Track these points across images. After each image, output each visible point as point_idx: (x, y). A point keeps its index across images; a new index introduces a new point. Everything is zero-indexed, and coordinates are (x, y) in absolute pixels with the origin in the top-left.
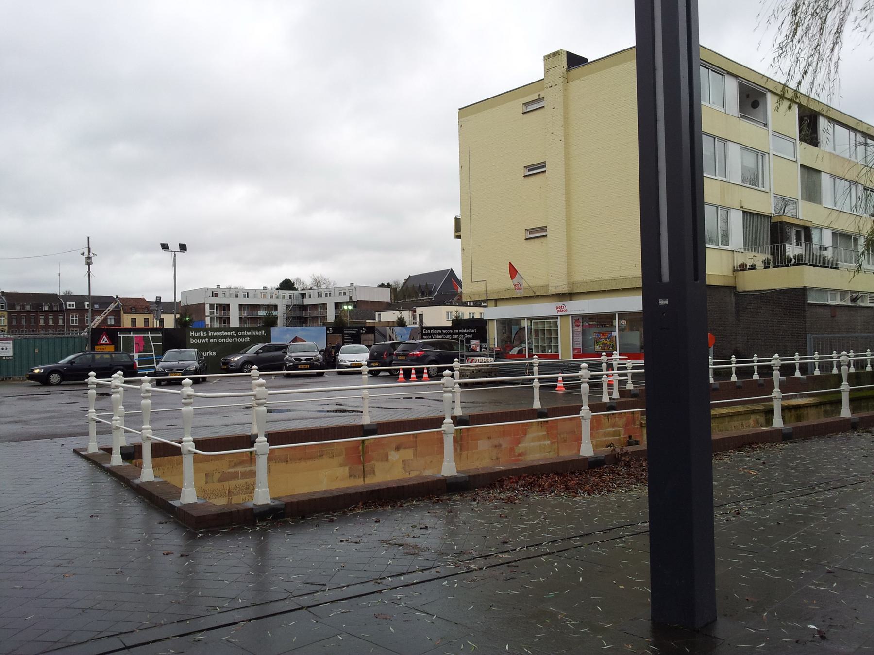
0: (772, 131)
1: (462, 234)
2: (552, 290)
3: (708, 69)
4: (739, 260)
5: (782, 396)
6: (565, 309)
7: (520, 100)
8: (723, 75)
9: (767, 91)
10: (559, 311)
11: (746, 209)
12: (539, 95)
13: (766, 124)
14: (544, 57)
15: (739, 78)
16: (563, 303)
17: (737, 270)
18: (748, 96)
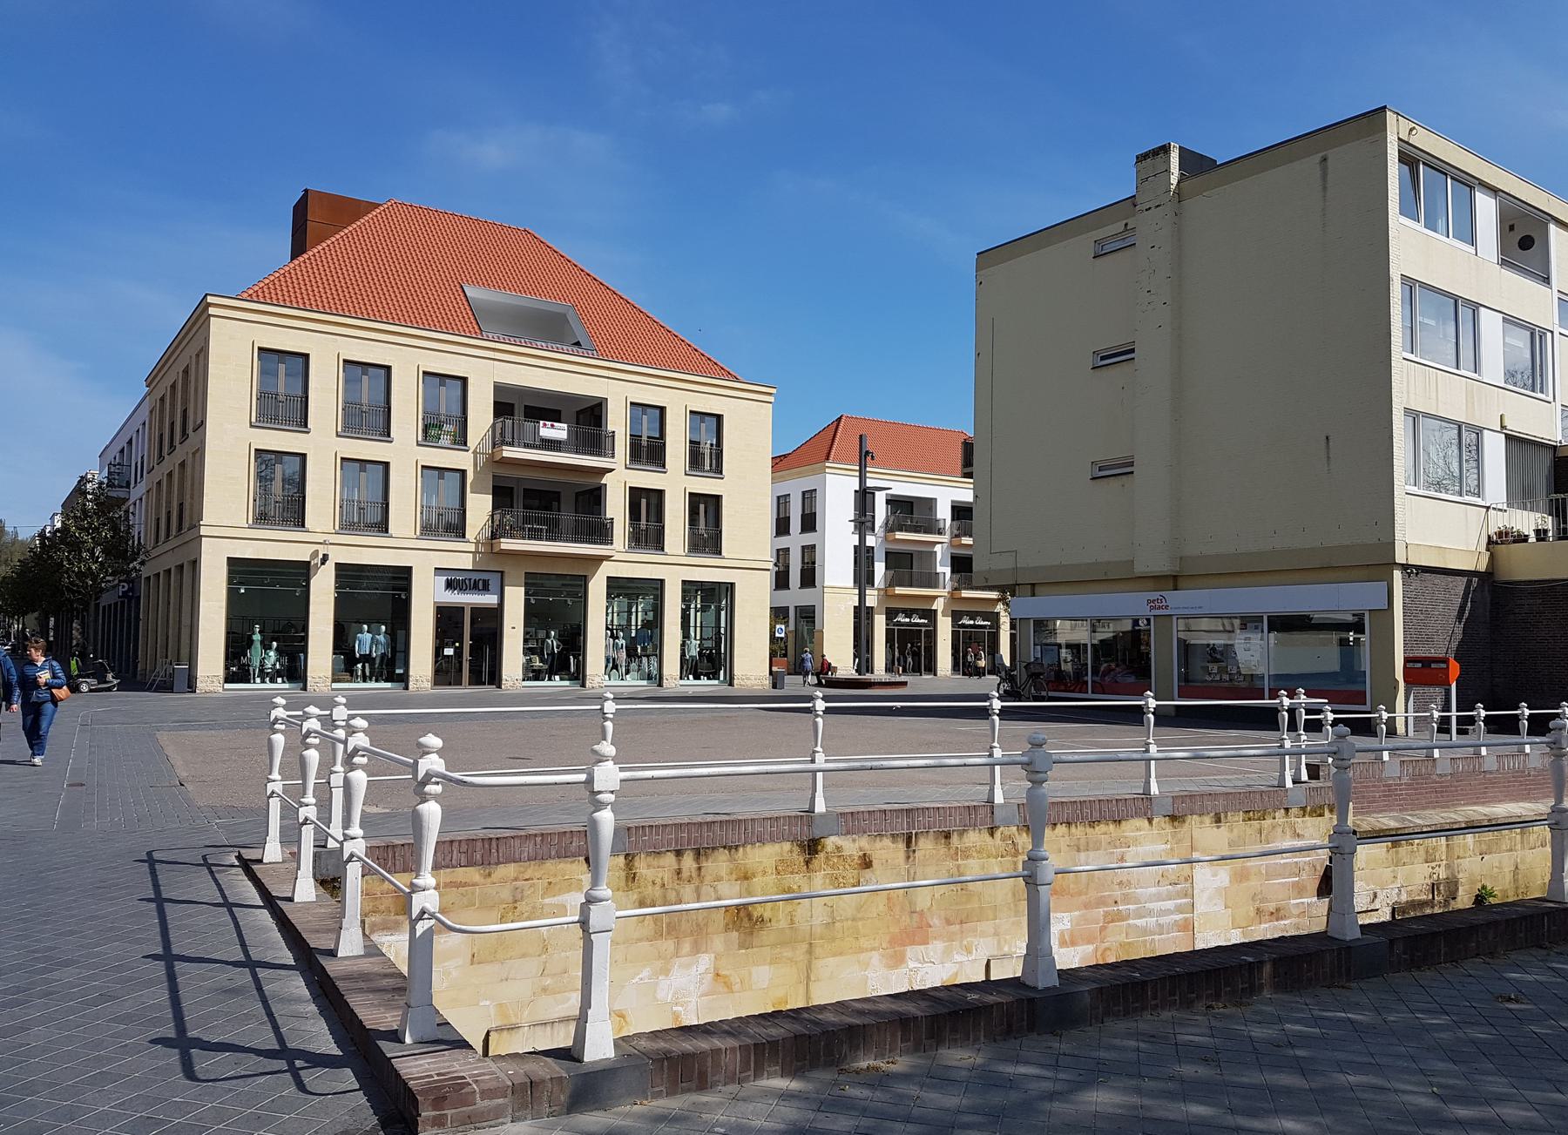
0: (1559, 291)
1: (975, 469)
2: (1140, 568)
3: (1446, 174)
4: (1498, 522)
5: (616, 709)
6: (1164, 603)
7: (1089, 234)
8: (1471, 187)
9: (1549, 218)
10: (1152, 608)
11: (1512, 431)
12: (1126, 225)
13: (1548, 278)
14: (1137, 157)
15: (1501, 193)
16: (1161, 593)
17: (1497, 543)
18: (1512, 228)
